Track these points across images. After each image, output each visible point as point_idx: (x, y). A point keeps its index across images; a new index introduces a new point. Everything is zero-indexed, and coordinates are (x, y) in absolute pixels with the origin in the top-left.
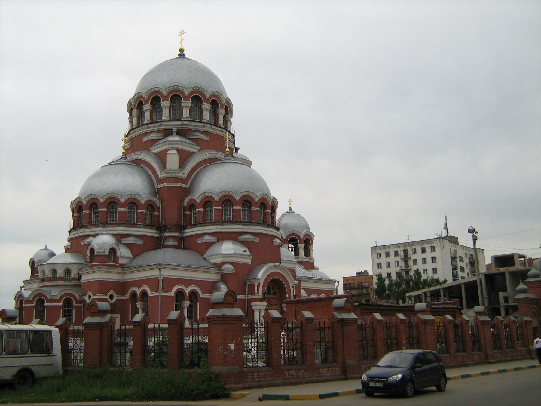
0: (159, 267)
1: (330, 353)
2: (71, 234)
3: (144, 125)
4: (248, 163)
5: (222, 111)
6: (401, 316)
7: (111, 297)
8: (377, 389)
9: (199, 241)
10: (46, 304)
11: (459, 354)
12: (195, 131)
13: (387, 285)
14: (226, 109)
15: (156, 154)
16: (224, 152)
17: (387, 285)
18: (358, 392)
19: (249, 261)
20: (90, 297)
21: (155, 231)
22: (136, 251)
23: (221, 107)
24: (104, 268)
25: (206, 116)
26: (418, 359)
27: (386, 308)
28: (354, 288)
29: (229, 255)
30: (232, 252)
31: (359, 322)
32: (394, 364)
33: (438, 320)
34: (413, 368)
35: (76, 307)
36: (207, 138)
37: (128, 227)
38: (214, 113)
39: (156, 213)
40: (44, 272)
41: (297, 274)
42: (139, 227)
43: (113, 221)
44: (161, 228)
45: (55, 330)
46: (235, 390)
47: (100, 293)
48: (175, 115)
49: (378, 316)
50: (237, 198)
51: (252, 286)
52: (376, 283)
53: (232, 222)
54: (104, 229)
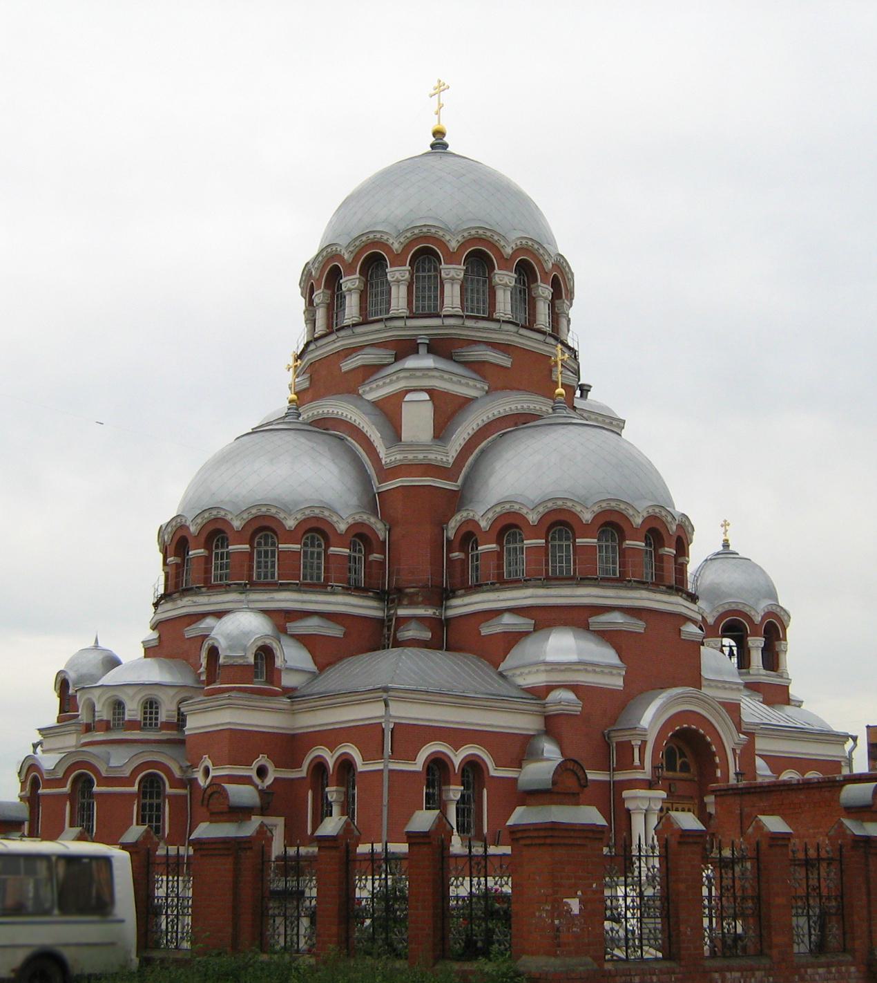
0: (385, 695)
1: (834, 928)
2: (160, 609)
3: (343, 328)
5: (544, 291)
7: (262, 772)
10: (96, 789)
14: (556, 284)
15: (376, 404)
16: (548, 392)
19: (617, 682)
20: (207, 772)
22: (326, 654)
23: (540, 279)
25: (504, 304)
30: (573, 658)
35: (173, 798)
36: (505, 361)
37: (305, 592)
38: (525, 298)
39: (375, 556)
40: (92, 708)
42: (333, 593)
44: (389, 595)
45: (120, 856)
48: (425, 299)
51: (626, 748)
53: (572, 578)
54: (242, 597)
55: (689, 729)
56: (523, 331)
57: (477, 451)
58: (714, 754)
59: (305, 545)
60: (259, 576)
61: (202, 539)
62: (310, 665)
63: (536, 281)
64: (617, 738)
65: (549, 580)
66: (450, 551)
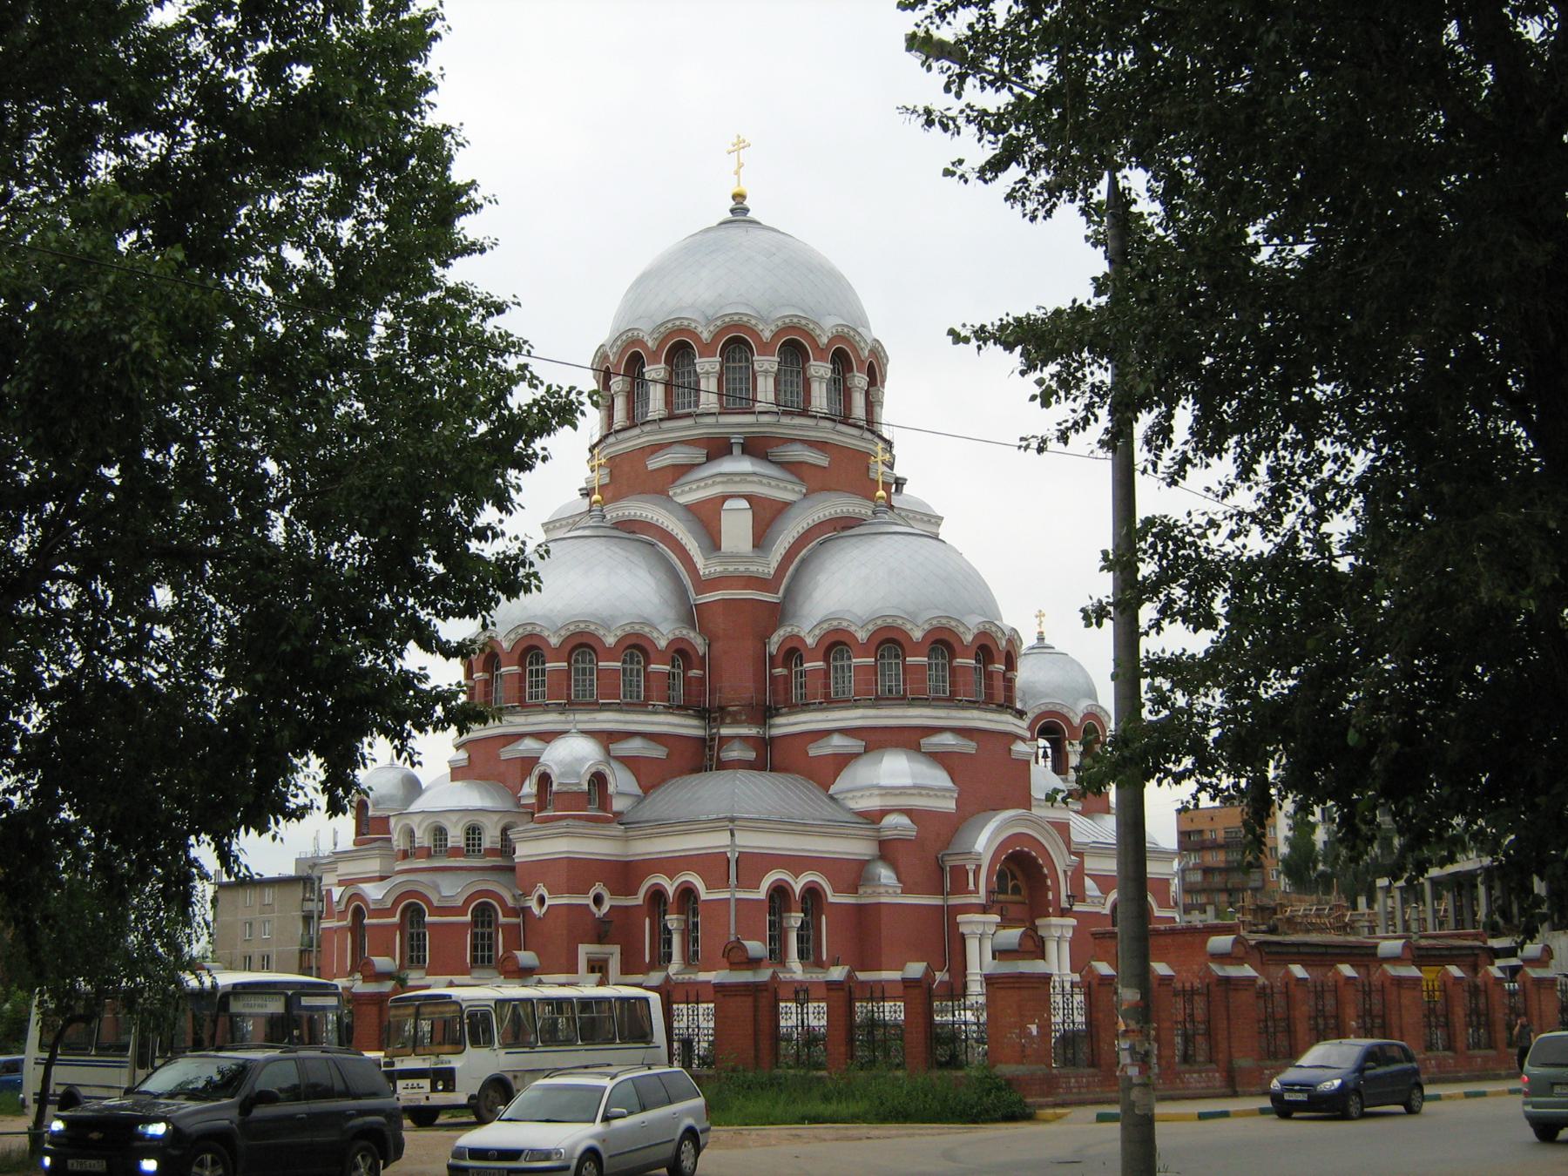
0: (731, 826)
1: (1201, 1042)
4: (927, 524)
5: (860, 380)
6: (1347, 970)
7: (598, 900)
8: (1298, 1106)
9: (814, 751)
10: (427, 919)
11: (1476, 1052)
12: (793, 441)
13: (1319, 845)
15: (688, 508)
16: (870, 497)
17: (1319, 845)
18: (1263, 1111)
19: (950, 805)
20: (542, 900)
21: (695, 722)
22: (651, 777)
23: (857, 365)
24: (584, 827)
25: (820, 398)
26: (1370, 1056)
27: (1315, 950)
28: (1214, 846)
29: (901, 791)
30: (908, 782)
31: (1261, 981)
32: (1328, 1061)
33: (1433, 976)
34: (1360, 1070)
35: (506, 927)
36: (820, 459)
37: (627, 712)
38: (840, 388)
41: (1076, 837)
42: (655, 713)
43: (584, 696)
44: (710, 714)
45: (655, 998)
46: (1041, 1106)
47: (572, 891)
48: (737, 396)
49: (1298, 971)
50: (917, 635)
51: (960, 874)
52: (1287, 838)
53: (904, 698)
54: (562, 718)
55: (1021, 852)
56: (841, 427)
57: (797, 560)
58: (1046, 877)
59: (624, 662)
60: (577, 696)
61: (516, 656)
62: (637, 790)
63: (851, 370)
64: (950, 862)
65: (878, 701)
66: (772, 666)
